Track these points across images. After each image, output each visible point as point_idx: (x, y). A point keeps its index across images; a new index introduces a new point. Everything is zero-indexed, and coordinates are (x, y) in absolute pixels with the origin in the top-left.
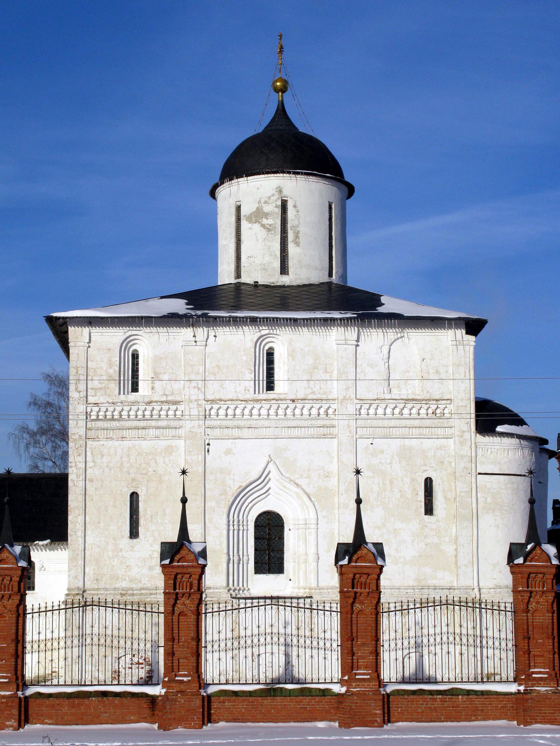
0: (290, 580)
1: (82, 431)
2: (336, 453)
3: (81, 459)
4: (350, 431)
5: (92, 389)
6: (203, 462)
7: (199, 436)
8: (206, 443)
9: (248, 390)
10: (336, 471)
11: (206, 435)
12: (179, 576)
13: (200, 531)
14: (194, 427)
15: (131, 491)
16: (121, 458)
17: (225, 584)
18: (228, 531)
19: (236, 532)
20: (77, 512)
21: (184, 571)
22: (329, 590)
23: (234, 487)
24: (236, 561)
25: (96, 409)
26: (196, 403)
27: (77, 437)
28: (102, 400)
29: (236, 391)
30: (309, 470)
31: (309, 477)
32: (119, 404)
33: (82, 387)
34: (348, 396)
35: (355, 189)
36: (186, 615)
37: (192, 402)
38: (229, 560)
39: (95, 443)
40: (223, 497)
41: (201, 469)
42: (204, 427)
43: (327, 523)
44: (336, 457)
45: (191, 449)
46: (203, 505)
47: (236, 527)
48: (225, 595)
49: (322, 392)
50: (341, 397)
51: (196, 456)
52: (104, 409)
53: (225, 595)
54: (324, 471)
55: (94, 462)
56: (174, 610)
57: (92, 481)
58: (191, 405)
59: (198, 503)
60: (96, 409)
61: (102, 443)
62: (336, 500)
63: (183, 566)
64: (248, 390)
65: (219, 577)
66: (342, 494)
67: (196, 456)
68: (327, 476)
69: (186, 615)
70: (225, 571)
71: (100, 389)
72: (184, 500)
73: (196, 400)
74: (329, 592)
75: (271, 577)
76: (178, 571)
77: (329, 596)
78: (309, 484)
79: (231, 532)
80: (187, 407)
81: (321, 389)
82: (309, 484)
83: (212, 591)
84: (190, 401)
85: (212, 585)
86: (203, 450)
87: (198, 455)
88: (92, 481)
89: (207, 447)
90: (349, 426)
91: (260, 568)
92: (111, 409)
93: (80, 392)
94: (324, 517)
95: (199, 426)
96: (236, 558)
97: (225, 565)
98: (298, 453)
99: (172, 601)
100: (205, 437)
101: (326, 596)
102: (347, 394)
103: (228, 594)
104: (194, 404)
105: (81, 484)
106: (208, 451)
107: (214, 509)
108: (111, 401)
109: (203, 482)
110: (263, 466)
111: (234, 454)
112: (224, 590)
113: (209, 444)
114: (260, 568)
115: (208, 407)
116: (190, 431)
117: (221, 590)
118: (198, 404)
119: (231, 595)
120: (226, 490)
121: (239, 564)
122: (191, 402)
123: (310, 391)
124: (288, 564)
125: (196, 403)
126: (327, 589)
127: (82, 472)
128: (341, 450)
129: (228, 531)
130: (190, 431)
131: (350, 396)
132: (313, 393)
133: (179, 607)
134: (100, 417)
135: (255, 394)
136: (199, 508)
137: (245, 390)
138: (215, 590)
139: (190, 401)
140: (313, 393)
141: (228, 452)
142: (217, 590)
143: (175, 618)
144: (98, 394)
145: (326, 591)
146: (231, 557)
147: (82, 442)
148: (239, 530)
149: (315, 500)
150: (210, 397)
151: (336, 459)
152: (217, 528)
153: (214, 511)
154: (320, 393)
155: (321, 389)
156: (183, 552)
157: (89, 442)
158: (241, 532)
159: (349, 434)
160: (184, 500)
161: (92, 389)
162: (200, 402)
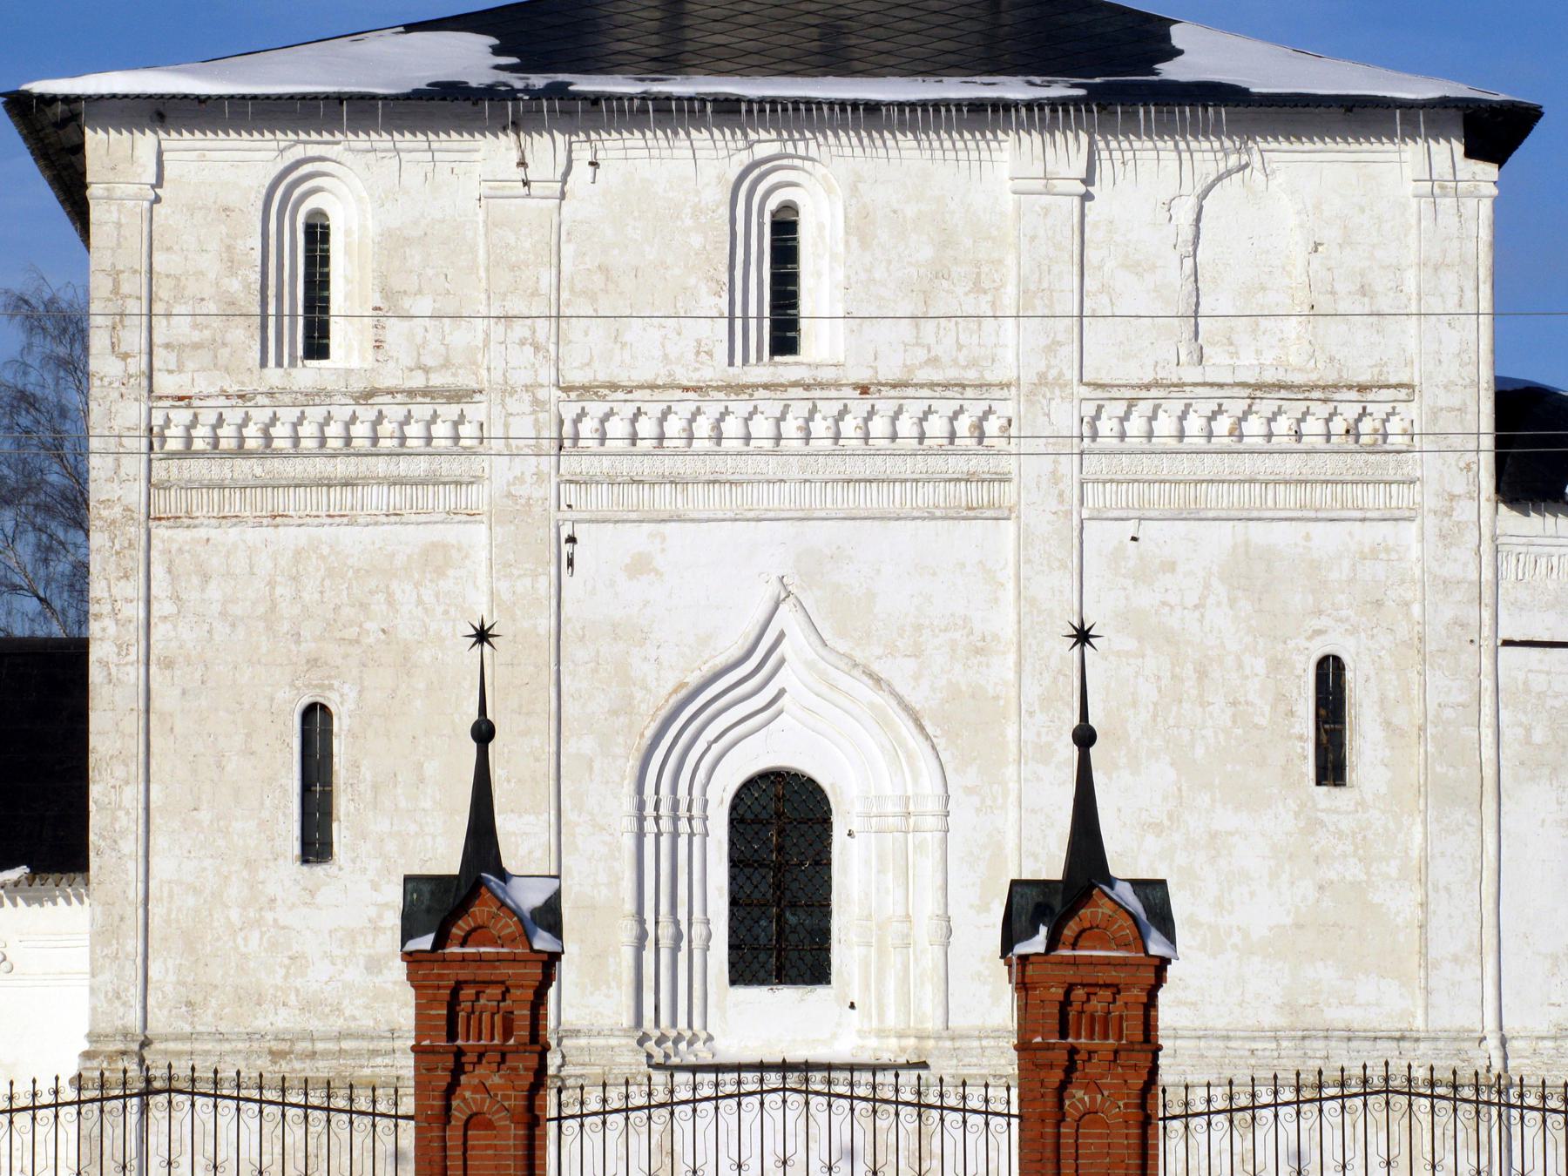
0: (852, 1006)
1: (135, 494)
2: (1011, 571)
3: (132, 588)
4: (1061, 494)
5: (167, 346)
7: (537, 509)
8: (564, 536)
9: (710, 354)
10: (1009, 633)
11: (564, 507)
12: (467, 992)
14: (520, 480)
15: (306, 700)
16: (272, 584)
17: (627, 1020)
19: (665, 842)
20: (120, 771)
21: (485, 973)
22: (985, 1043)
24: (665, 943)
25: (181, 417)
26: (527, 397)
27: (117, 511)
28: (202, 385)
30: (918, 628)
32: (261, 400)
33: (134, 338)
34: (1053, 373)
36: (489, 1125)
39: (181, 535)
41: (546, 624)
43: (978, 810)
45: (511, 557)
46: (553, 748)
47: (665, 825)
48: (627, 1058)
50: (1028, 377)
51: (528, 581)
52: (208, 417)
55: (177, 598)
56: (448, 1108)
57: (169, 664)
60: (181, 417)
61: (202, 533)
62: (1011, 732)
63: (479, 959)
65: (607, 996)
66: (1031, 714)
67: (528, 581)
68: (978, 651)
69: (489, 1125)
71: (196, 346)
72: (483, 733)
73: (527, 387)
74: (983, 1049)
75: (788, 994)
76: (464, 974)
77: (985, 1061)
78: (917, 677)
79: (649, 842)
80: (497, 410)
81: (960, 347)
82: (917, 677)
83: (583, 1042)
84: (508, 391)
87: (535, 576)
88: (169, 664)
89: (566, 548)
92: (234, 416)
93: (125, 356)
94: (969, 791)
95: (539, 476)
96: (666, 931)
97: (628, 954)
98: (879, 571)
99: (442, 1078)
100: (560, 515)
101: (974, 1060)
102: (1049, 367)
104: (520, 400)
105: (132, 674)
106: (570, 563)
107: (591, 760)
108: (233, 389)
110: (760, 614)
112: (624, 1041)
113: (572, 540)
114: (748, 966)
115: (570, 411)
116: (509, 495)
117: (613, 1042)
118: (536, 402)
119: (649, 1056)
120: (631, 697)
121: (675, 950)
123: (922, 354)
125: (527, 397)
126: (980, 1038)
127: (133, 633)
128: (1028, 561)
132: (934, 361)
133: (467, 1099)
134: (198, 445)
135: (731, 364)
136: (537, 760)
137: (698, 353)
138: (594, 1042)
139: (508, 391)
140: (934, 361)
141: (640, 566)
142: (601, 1042)
143: (454, 1135)
144: (190, 365)
145: (975, 1044)
147: (135, 532)
148: (675, 835)
150: (575, 376)
151: (1010, 593)
153: (591, 769)
155: (960, 347)
156: (480, 912)
157: (160, 532)
158: (683, 842)
159: (1053, 505)
160: (483, 733)
161: (167, 346)
162: (542, 394)
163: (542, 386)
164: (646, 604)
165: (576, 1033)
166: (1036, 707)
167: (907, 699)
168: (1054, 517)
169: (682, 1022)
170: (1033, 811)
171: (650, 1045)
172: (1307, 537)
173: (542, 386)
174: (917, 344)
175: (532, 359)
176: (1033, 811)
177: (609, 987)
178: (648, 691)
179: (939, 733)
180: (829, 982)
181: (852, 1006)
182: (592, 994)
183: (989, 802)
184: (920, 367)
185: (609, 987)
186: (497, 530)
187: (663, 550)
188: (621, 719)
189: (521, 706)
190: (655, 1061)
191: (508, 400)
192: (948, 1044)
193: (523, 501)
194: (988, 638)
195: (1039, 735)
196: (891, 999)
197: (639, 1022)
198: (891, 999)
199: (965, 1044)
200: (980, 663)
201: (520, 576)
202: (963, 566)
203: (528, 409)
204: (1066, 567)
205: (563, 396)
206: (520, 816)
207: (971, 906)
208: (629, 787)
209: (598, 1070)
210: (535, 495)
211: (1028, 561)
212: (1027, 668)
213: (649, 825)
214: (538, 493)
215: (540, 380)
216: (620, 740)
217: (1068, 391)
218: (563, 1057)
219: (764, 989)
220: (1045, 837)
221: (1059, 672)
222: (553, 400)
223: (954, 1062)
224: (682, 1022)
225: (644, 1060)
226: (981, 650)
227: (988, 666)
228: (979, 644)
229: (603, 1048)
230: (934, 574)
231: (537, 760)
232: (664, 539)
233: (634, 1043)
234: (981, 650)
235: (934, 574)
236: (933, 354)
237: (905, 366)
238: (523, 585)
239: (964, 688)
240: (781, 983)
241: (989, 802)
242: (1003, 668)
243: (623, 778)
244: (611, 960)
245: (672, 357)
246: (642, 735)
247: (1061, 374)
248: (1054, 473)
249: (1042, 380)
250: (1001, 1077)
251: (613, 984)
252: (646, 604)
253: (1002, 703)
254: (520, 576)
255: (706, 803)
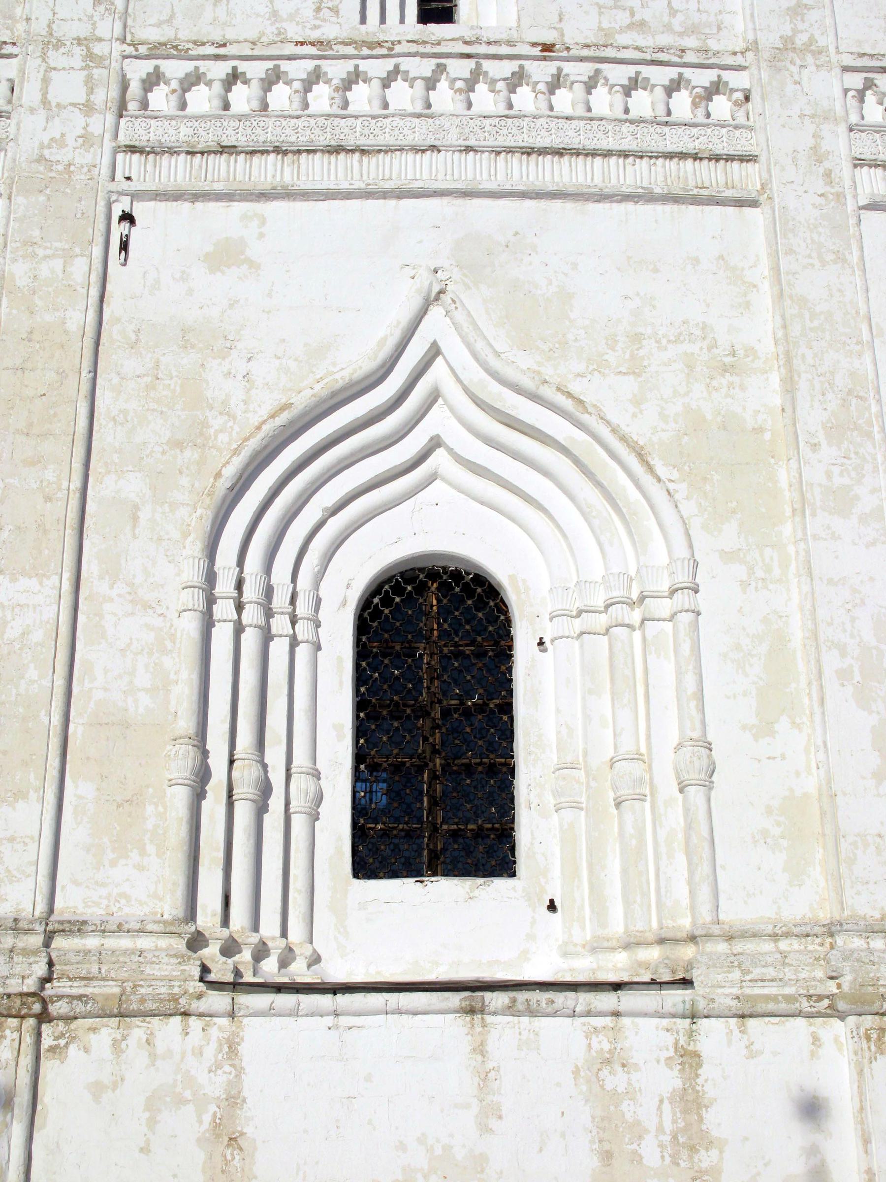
0: (552, 907)
2: (764, 267)
4: (828, 174)
6: (94, 292)
7: (80, 177)
8: (116, 213)
9: (335, 11)
10: (767, 347)
11: (119, 176)
13: (49, 613)
14: (60, 142)
17: (171, 906)
18: (208, 623)
19: (250, 640)
22: (783, 945)
23: (252, 405)
24: (245, 790)
26: (78, 51)
29: (275, 14)
30: (637, 338)
31: (636, 370)
34: (801, 39)
35: (499, 571)
37: (59, 44)
38: (202, 776)
40: (190, 454)
41: (79, 318)
42: (108, 145)
43: (744, 585)
44: (766, 287)
45: (36, 233)
46: (76, 483)
47: (252, 615)
48: (167, 968)
49: (677, 23)
50: (769, 40)
51: (57, 264)
53: (167, 968)
54: (714, 345)
58: (56, 58)
59: (50, 475)
62: (783, 476)
64: (335, 11)
65: (140, 868)
66: (815, 447)
67: (57, 264)
68: (726, 369)
70: (179, 833)
73: (79, 41)
74: (784, 955)
75: (446, 890)
77: (789, 974)
78: (638, 401)
79: (222, 636)
80: (33, 63)
81: (673, 12)
82: (638, 401)
83: (92, 942)
84: (52, 42)
85: (93, 913)
86: (100, 240)
87: (68, 257)
89: (118, 230)
90: (818, 156)
91: (381, 849)
94: (729, 557)
95: (87, 140)
96: (246, 776)
97: (180, 797)
98: (575, 266)
100: (113, 187)
101: (771, 972)
102: (795, 31)
103: (183, 959)
104: (69, 54)
106: (124, 246)
107: (136, 507)
109: (86, 376)
110: (403, 314)
111: (253, 265)
112: (164, 942)
113: (128, 218)
114: (381, 849)
115: (138, 70)
116: (41, 159)
117: (144, 943)
118: (90, 56)
119: (205, 970)
120: (205, 424)
121: (261, 809)
122: (56, 47)
123: (623, 18)
124: (536, 824)
125: (78, 51)
126: (775, 937)
128: (790, 252)
129: (208, 623)
130: (41, 159)
131: (812, 40)
132: (641, 26)
135: (363, 20)
136: (48, 499)
137: (318, 9)
138: (111, 942)
139: (52, 42)
140: (641, 26)
141: (225, 256)
142: (124, 942)
145: (767, 946)
146: (218, 763)
148: (267, 637)
149: (675, 475)
150: (150, 33)
151: (765, 298)
152: (147, 606)
153: (135, 519)
154: (668, 28)
155: (673, 12)
158: (279, 649)
159: (820, 186)
162: (99, 49)
163: (100, 40)
164: (233, 304)
165: (78, 927)
166: (821, 438)
167: (625, 429)
168: (821, 200)
169: (270, 926)
170: (830, 582)
171: (211, 952)
172: (675, 1023)
173: (100, 40)
174: (616, 7)
175: (90, 11)
176: (830, 582)
177: (143, 852)
178: (232, 416)
179: (675, 475)
180: (513, 875)
181: (552, 907)
182: (113, 864)
183: (760, 573)
184: (621, 31)
185: (143, 852)
186: (20, 200)
187: (261, 236)
188: (188, 453)
189: (30, 425)
190: (212, 977)
191: (50, 53)
192: (722, 947)
193: (60, 168)
194: (741, 353)
195: (829, 475)
196: (614, 889)
197: (191, 913)
198: (614, 889)
199: (750, 946)
200: (731, 385)
201: (46, 257)
202: (696, 261)
203: (78, 63)
204: (844, 261)
205: (130, 50)
206: (14, 580)
207: (744, 728)
208: (195, 547)
209: (114, 989)
210: (78, 160)
211: (790, 252)
212: (803, 385)
213: (224, 609)
214: (83, 158)
215: (99, 33)
216: (184, 481)
217: (823, 58)
218: (51, 964)
219: (409, 883)
220: (853, 620)
221: (850, 392)
222: (116, 55)
223: (736, 975)
224: (270, 926)
225: (196, 972)
226: (731, 366)
227: (743, 388)
228: (728, 360)
229: (125, 952)
230: (656, 270)
231: (48, 499)
232: (263, 221)
233: (180, 945)
234: (731, 366)
235: (656, 270)
236: (637, 17)
237: (600, 29)
238: (51, 268)
239: (709, 417)
240: (435, 874)
241: (760, 573)
242: (763, 393)
243: (186, 535)
244: (150, 809)
245: (283, 14)
246: (218, 475)
247: (812, 40)
248: (815, 148)
249: (788, 45)
250: (820, 998)
251: (151, 849)
252: (233, 304)
253: (767, 436)
254: (46, 257)
255: (318, 603)
